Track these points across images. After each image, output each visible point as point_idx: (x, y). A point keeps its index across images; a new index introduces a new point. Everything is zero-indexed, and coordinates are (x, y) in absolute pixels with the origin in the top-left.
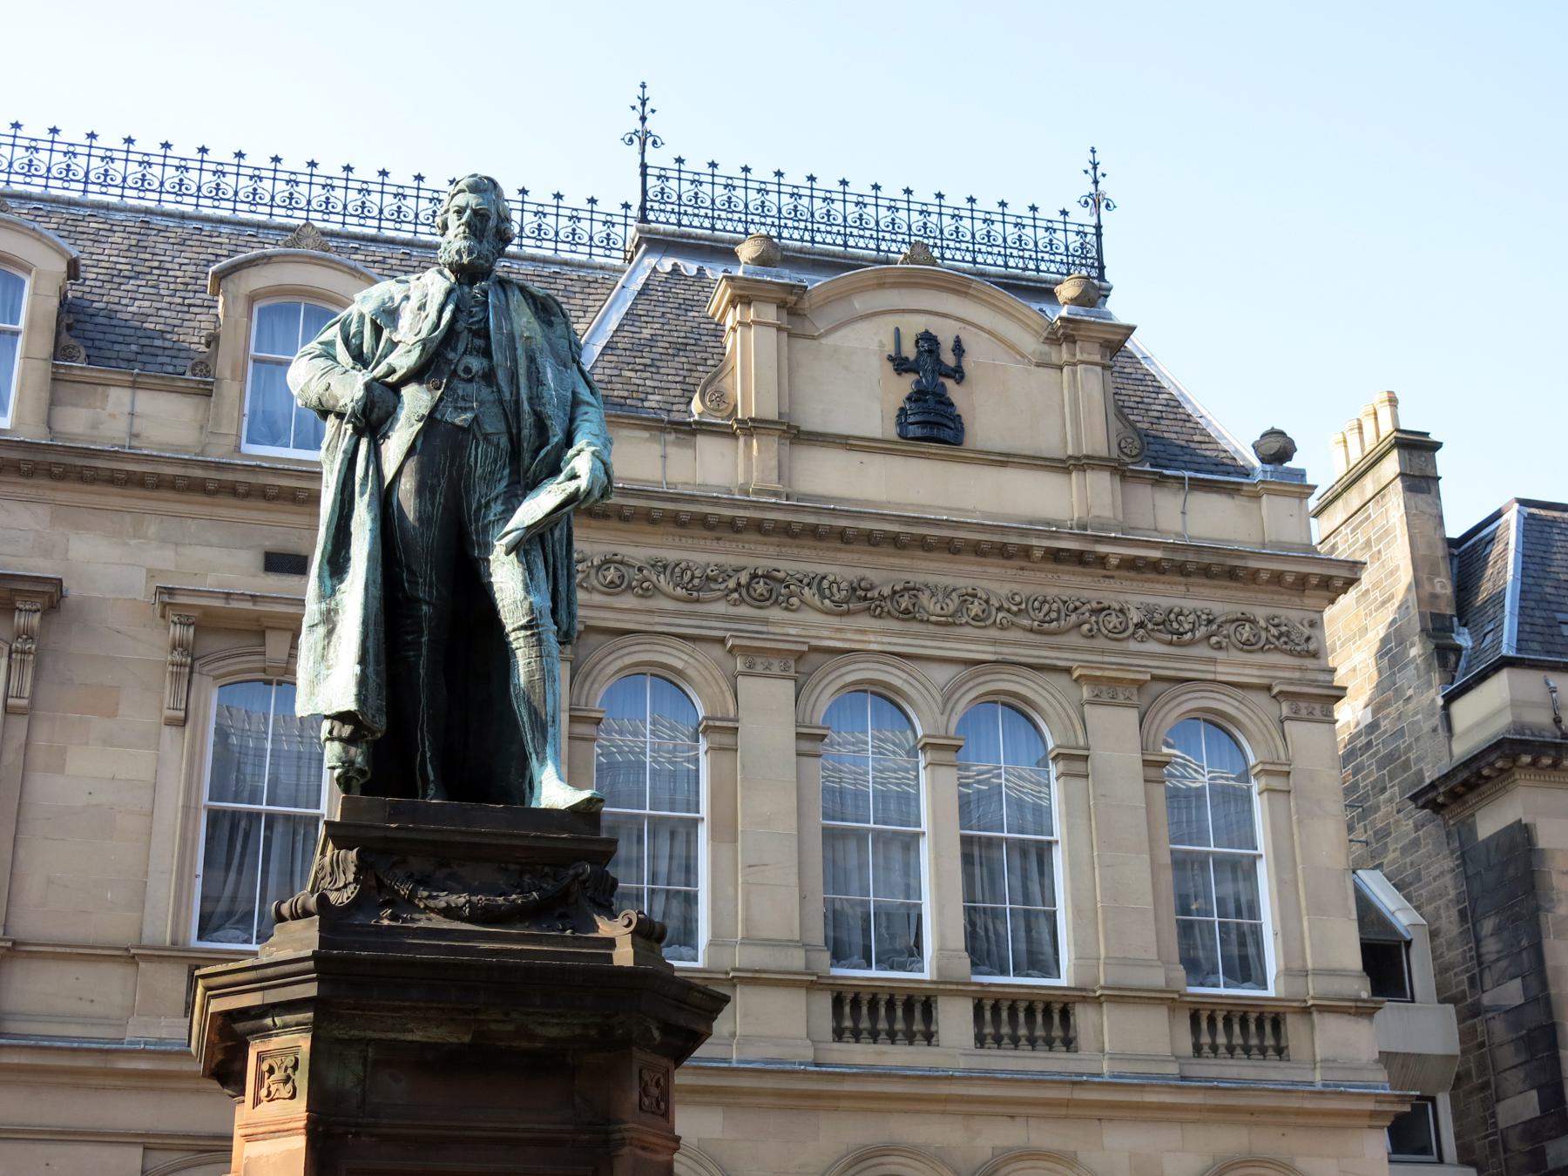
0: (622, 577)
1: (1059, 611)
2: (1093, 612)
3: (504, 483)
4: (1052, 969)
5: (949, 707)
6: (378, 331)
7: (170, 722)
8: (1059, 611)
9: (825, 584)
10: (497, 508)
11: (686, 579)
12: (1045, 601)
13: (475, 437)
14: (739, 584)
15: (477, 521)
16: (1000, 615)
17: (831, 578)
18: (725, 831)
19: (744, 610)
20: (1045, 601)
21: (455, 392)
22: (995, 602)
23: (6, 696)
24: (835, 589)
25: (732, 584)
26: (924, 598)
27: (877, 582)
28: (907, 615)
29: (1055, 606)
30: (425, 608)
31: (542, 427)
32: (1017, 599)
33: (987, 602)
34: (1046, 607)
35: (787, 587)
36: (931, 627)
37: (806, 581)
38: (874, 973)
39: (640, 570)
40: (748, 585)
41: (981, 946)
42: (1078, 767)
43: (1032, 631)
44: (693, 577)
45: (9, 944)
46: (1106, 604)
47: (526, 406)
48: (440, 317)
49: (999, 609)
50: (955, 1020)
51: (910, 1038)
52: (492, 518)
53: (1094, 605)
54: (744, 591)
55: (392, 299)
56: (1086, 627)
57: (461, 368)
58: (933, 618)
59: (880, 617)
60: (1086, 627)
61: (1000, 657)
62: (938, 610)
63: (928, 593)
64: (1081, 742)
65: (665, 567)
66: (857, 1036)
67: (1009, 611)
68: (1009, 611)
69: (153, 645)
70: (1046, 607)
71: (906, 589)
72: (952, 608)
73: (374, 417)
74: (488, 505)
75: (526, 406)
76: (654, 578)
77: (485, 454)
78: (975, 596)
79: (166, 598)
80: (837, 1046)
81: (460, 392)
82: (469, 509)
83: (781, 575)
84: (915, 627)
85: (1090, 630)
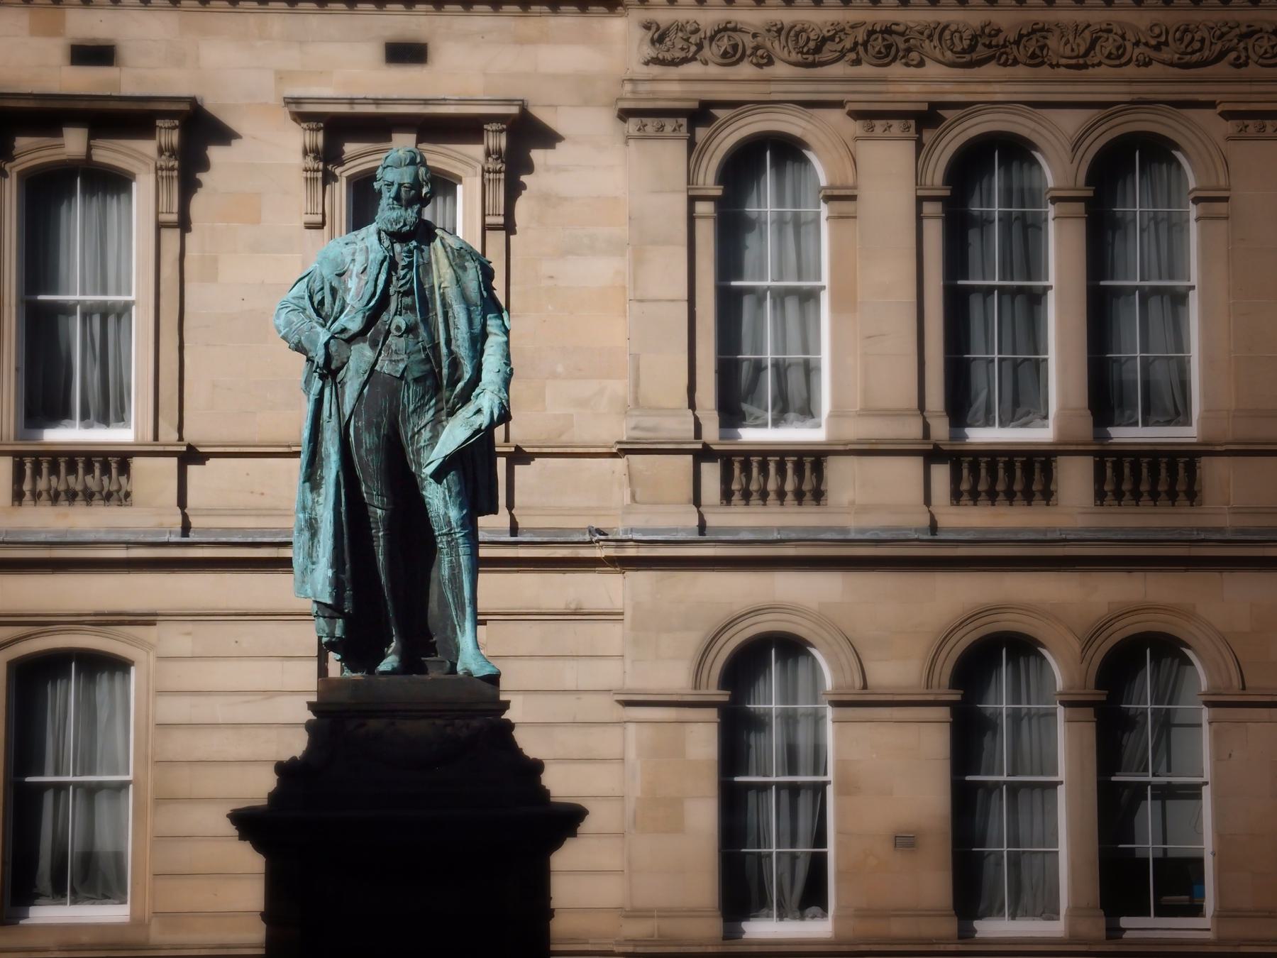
0: (735, 47)
1: (1203, 41)
2: (1242, 37)
3: (431, 412)
4: (1180, 415)
5: (1079, 154)
6: (334, 291)
7: (310, 226)
8: (1203, 41)
9: (947, 34)
10: (426, 434)
11: (801, 42)
12: (1186, 30)
13: (407, 383)
14: (856, 44)
15: (412, 444)
16: (1137, 51)
17: (953, 27)
18: (843, 303)
19: (866, 70)
20: (1186, 30)
21: (389, 347)
22: (1131, 37)
23: (157, 213)
24: (957, 41)
25: (848, 44)
26: (1052, 42)
27: (1004, 26)
28: (1036, 60)
29: (1197, 37)
30: (379, 511)
31: (455, 364)
32: (1157, 30)
33: (1123, 37)
34: (1188, 37)
35: (907, 41)
36: (1062, 70)
37: (927, 32)
38: (1052, 356)
39: (755, 36)
40: (865, 44)
41: (1104, 395)
42: (1220, 208)
43: (1172, 65)
44: (808, 39)
45: (184, 449)
46: (1257, 27)
47: (444, 350)
48: (376, 286)
49: (1137, 44)
50: (1075, 479)
51: (1028, 497)
52: (422, 444)
53: (1244, 29)
54: (861, 49)
55: (343, 261)
56: (1233, 55)
57: (393, 327)
58: (1063, 61)
59: (1005, 65)
60: (1233, 55)
61: (1135, 97)
62: (1068, 52)
63: (1057, 32)
64: (1222, 182)
65: (779, 31)
66: (974, 496)
67: (1146, 44)
68: (1146, 44)
69: (290, 145)
70: (1188, 37)
71: (1034, 31)
72: (1082, 50)
73: (333, 367)
74: (419, 431)
75: (444, 350)
76: (768, 44)
77: (416, 393)
78: (1110, 31)
79: (294, 108)
80: (955, 510)
81: (393, 347)
82: (406, 433)
83: (901, 29)
84: (1045, 71)
85: (1238, 58)
